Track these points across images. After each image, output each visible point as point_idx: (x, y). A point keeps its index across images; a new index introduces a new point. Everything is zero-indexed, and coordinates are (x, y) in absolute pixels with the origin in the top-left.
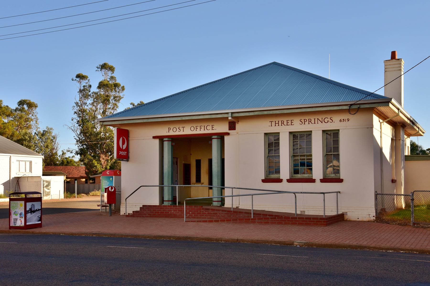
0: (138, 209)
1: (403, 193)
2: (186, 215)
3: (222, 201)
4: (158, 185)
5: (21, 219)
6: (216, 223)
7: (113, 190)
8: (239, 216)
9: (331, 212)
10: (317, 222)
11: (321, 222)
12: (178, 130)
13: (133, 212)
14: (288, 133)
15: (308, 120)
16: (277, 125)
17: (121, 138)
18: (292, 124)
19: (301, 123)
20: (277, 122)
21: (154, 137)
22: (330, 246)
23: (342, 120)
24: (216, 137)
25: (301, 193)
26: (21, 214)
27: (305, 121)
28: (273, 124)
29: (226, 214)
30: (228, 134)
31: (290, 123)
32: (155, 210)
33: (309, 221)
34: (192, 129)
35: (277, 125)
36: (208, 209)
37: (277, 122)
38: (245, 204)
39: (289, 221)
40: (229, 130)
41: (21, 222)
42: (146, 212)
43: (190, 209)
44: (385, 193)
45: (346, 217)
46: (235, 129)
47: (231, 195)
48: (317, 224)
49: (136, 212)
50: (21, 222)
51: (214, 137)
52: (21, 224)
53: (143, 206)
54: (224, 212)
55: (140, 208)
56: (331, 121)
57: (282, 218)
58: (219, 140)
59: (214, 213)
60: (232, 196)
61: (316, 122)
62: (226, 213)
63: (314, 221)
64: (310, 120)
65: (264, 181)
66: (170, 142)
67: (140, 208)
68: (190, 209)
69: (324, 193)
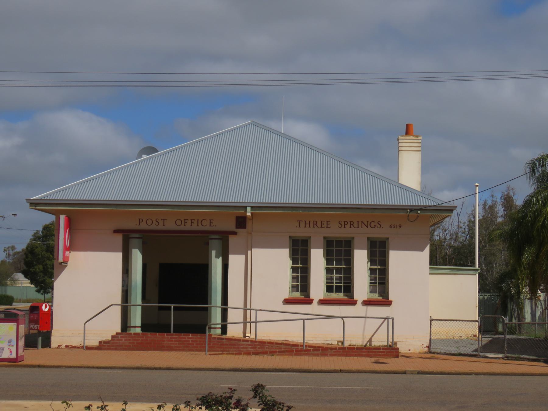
3: (224, 329)
4: (120, 303)
5: (11, 348)
7: (47, 309)
9: (380, 340)
12: (155, 222)
13: (100, 342)
14: (235, 218)
15: (349, 223)
19: (340, 226)
20: (307, 222)
23: (393, 226)
26: (10, 341)
27: (346, 223)
28: (303, 224)
30: (235, 233)
32: (118, 340)
34: (179, 223)
37: (307, 222)
38: (266, 332)
40: (237, 227)
41: (11, 352)
43: (193, 338)
46: (245, 228)
47: (258, 320)
48: (388, 356)
50: (11, 352)
52: (11, 354)
56: (379, 226)
57: (296, 351)
59: (230, 345)
61: (360, 226)
62: (249, 343)
64: (352, 223)
65: (287, 302)
66: (141, 240)
68: (193, 338)
69: (342, 318)
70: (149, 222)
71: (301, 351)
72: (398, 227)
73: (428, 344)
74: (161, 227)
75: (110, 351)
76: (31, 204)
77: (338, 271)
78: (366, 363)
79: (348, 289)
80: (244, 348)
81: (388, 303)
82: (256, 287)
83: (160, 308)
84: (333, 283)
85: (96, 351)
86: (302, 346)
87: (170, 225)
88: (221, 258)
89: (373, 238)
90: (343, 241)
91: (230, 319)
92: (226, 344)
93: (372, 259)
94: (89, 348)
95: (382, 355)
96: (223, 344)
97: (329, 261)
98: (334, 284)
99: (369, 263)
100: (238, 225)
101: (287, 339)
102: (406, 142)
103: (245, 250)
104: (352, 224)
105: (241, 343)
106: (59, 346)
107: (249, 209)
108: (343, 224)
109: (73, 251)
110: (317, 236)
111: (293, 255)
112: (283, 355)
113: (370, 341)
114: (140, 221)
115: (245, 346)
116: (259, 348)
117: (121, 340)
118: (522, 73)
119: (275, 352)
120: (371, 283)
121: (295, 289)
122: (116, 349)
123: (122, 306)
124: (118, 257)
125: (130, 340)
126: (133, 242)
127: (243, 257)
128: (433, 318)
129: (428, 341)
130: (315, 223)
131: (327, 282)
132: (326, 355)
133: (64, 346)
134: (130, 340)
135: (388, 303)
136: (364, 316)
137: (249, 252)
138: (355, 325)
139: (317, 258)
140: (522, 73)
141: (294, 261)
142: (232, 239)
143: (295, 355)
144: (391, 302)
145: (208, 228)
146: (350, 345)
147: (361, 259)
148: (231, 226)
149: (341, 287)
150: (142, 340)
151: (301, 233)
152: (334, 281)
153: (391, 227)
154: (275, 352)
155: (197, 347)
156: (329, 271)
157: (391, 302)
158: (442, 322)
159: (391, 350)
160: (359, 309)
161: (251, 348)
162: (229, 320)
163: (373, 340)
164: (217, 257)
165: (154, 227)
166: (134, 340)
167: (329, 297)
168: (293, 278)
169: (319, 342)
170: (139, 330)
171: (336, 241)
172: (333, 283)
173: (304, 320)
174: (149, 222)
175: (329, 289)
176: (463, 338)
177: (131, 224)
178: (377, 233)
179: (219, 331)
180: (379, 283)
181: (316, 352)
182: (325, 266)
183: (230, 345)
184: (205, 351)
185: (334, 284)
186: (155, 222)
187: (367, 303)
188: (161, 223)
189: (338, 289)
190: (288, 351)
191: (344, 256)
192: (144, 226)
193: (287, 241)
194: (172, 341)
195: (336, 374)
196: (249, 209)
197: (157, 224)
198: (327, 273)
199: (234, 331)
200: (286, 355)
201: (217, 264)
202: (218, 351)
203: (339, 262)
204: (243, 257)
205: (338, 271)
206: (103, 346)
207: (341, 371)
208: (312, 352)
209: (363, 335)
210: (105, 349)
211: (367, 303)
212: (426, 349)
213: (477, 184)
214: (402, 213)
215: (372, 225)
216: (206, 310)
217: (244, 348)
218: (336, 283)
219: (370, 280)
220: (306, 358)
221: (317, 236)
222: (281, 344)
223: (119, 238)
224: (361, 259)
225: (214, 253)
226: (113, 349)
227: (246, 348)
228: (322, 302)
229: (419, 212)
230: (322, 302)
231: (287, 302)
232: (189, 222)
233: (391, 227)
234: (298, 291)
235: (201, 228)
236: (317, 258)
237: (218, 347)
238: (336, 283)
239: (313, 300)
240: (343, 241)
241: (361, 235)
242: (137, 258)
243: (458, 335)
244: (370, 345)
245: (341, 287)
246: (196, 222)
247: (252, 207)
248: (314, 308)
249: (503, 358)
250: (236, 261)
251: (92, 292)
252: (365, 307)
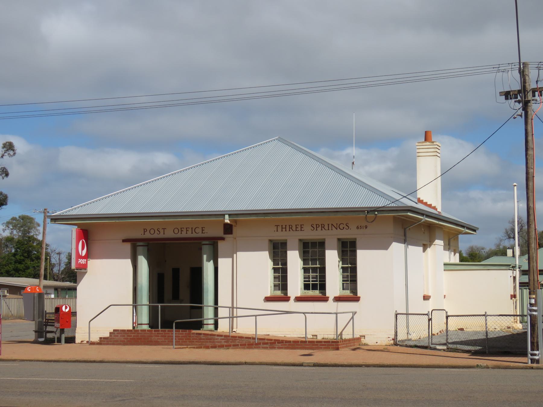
0: (107, 335)
1: (518, 314)
2: (176, 339)
4: (132, 303)
6: (214, 350)
7: (67, 310)
8: (234, 341)
10: (328, 345)
11: (333, 345)
12: (156, 231)
13: (101, 338)
14: (297, 241)
16: (284, 230)
17: (81, 242)
18: (302, 229)
19: (313, 229)
20: (284, 227)
21: (124, 241)
22: (264, 213)
24: (207, 242)
25: (312, 313)
28: (280, 228)
29: (223, 339)
30: (223, 239)
31: (299, 229)
32: (115, 336)
33: (320, 345)
34: (176, 231)
35: (284, 230)
36: (200, 334)
37: (284, 227)
38: (244, 327)
39: (298, 345)
40: (225, 234)
42: (118, 338)
44: (409, 313)
45: (363, 341)
46: (232, 234)
48: (329, 348)
49: (105, 338)
51: (204, 242)
53: (114, 330)
54: (220, 338)
55: (110, 333)
56: (347, 228)
58: (212, 247)
59: (207, 339)
60: (407, 314)
61: (330, 228)
62: (223, 338)
63: (325, 345)
65: (268, 299)
67: (110, 333)
69: (304, 313)
70: (152, 232)
71: (252, 344)
72: (364, 228)
73: (393, 337)
74: (161, 236)
75: (108, 346)
76: (51, 219)
77: (314, 270)
78: (294, 356)
79: (323, 287)
80: (218, 342)
81: (356, 299)
82: (242, 287)
83: (192, 307)
84: (309, 281)
85: (97, 346)
86: (254, 339)
87: (169, 234)
88: (212, 261)
89: (314, 239)
90: (321, 241)
91: (220, 315)
92: (204, 339)
93: (305, 257)
94: (92, 343)
95: (324, 348)
96: (201, 339)
97: (305, 261)
98: (311, 282)
99: (341, 262)
100: (219, 233)
101: (268, 334)
102: (424, 148)
103: (230, 255)
104: (323, 227)
105: (216, 337)
106: (82, 341)
107: (227, 217)
108: (315, 227)
109: (92, 258)
110: (293, 238)
111: (274, 256)
112: (237, 348)
113: (341, 334)
114: (145, 230)
115: (219, 340)
116: (231, 342)
117: (117, 336)
118: (433, 73)
119: (238, 345)
120: (343, 281)
121: (278, 288)
122: (113, 344)
123: (149, 306)
124: (128, 262)
125: (124, 336)
126: (140, 249)
127: (231, 259)
128: (398, 312)
129: (394, 333)
130: (291, 228)
131: (304, 281)
132: (274, 348)
133: (85, 342)
134: (124, 336)
135: (356, 299)
136: (405, 312)
137: (235, 255)
138: (318, 321)
139: (294, 260)
140: (433, 73)
141: (275, 262)
142: (221, 244)
143: (248, 348)
144: (359, 298)
145: (200, 235)
146: (323, 339)
147: (332, 258)
148: (219, 232)
149: (316, 284)
150: (134, 336)
151: (279, 236)
152: (311, 280)
153: (358, 228)
154: (230, 346)
155: (179, 342)
156: (306, 270)
157: (359, 298)
158: (469, 317)
159: (355, 344)
160: (330, 306)
161: (225, 342)
162: (220, 316)
163: (343, 333)
164: (208, 260)
165: (156, 236)
166: (128, 336)
167: (306, 294)
168: (275, 278)
169: (295, 336)
170: (146, 327)
171: (311, 243)
172: (309, 281)
173: (256, 316)
174: (152, 232)
175: (306, 287)
176: (496, 330)
177: (137, 234)
178: (346, 234)
179: (212, 327)
180: (351, 281)
181: (265, 346)
182: (302, 266)
183: (207, 339)
184: (173, 345)
185: (311, 282)
186: (156, 231)
187: (338, 299)
188: (162, 231)
189: (314, 287)
190: (241, 345)
191: (319, 256)
192: (148, 235)
193: (266, 244)
194: (159, 336)
195: (241, 366)
196: (227, 217)
197: (158, 233)
198: (304, 273)
199: (224, 327)
200: (239, 348)
201: (208, 267)
202: (197, 345)
203: (314, 261)
204: (231, 259)
205: (314, 270)
206: (103, 341)
207: (246, 363)
208: (262, 346)
209: (486, 328)
210: (104, 344)
211: (338, 299)
212: (392, 342)
213: (515, 184)
214: (362, 215)
215: (341, 227)
216: (201, 308)
217: (218, 342)
218: (312, 281)
219: (343, 278)
220: (256, 351)
221: (293, 238)
222: (250, 338)
223: (128, 247)
224: (332, 258)
225: (205, 257)
226: (110, 344)
227: (220, 342)
228: (299, 299)
229: (376, 213)
230: (299, 299)
231: (268, 299)
232: (185, 230)
233: (358, 228)
234: (279, 290)
235: (194, 235)
236: (294, 260)
237: (197, 342)
238: (312, 281)
239: (289, 297)
240: (321, 241)
241: (331, 237)
242: (143, 263)
243: (493, 327)
244: (341, 338)
245: (316, 284)
246: (190, 230)
247: (230, 215)
248: (291, 305)
249: (444, 350)
250: (224, 263)
251: (109, 294)
252: (336, 303)
